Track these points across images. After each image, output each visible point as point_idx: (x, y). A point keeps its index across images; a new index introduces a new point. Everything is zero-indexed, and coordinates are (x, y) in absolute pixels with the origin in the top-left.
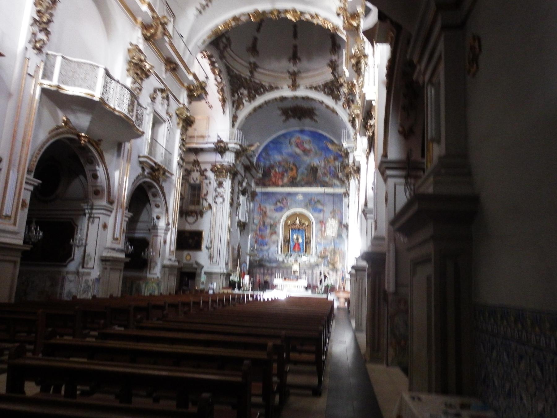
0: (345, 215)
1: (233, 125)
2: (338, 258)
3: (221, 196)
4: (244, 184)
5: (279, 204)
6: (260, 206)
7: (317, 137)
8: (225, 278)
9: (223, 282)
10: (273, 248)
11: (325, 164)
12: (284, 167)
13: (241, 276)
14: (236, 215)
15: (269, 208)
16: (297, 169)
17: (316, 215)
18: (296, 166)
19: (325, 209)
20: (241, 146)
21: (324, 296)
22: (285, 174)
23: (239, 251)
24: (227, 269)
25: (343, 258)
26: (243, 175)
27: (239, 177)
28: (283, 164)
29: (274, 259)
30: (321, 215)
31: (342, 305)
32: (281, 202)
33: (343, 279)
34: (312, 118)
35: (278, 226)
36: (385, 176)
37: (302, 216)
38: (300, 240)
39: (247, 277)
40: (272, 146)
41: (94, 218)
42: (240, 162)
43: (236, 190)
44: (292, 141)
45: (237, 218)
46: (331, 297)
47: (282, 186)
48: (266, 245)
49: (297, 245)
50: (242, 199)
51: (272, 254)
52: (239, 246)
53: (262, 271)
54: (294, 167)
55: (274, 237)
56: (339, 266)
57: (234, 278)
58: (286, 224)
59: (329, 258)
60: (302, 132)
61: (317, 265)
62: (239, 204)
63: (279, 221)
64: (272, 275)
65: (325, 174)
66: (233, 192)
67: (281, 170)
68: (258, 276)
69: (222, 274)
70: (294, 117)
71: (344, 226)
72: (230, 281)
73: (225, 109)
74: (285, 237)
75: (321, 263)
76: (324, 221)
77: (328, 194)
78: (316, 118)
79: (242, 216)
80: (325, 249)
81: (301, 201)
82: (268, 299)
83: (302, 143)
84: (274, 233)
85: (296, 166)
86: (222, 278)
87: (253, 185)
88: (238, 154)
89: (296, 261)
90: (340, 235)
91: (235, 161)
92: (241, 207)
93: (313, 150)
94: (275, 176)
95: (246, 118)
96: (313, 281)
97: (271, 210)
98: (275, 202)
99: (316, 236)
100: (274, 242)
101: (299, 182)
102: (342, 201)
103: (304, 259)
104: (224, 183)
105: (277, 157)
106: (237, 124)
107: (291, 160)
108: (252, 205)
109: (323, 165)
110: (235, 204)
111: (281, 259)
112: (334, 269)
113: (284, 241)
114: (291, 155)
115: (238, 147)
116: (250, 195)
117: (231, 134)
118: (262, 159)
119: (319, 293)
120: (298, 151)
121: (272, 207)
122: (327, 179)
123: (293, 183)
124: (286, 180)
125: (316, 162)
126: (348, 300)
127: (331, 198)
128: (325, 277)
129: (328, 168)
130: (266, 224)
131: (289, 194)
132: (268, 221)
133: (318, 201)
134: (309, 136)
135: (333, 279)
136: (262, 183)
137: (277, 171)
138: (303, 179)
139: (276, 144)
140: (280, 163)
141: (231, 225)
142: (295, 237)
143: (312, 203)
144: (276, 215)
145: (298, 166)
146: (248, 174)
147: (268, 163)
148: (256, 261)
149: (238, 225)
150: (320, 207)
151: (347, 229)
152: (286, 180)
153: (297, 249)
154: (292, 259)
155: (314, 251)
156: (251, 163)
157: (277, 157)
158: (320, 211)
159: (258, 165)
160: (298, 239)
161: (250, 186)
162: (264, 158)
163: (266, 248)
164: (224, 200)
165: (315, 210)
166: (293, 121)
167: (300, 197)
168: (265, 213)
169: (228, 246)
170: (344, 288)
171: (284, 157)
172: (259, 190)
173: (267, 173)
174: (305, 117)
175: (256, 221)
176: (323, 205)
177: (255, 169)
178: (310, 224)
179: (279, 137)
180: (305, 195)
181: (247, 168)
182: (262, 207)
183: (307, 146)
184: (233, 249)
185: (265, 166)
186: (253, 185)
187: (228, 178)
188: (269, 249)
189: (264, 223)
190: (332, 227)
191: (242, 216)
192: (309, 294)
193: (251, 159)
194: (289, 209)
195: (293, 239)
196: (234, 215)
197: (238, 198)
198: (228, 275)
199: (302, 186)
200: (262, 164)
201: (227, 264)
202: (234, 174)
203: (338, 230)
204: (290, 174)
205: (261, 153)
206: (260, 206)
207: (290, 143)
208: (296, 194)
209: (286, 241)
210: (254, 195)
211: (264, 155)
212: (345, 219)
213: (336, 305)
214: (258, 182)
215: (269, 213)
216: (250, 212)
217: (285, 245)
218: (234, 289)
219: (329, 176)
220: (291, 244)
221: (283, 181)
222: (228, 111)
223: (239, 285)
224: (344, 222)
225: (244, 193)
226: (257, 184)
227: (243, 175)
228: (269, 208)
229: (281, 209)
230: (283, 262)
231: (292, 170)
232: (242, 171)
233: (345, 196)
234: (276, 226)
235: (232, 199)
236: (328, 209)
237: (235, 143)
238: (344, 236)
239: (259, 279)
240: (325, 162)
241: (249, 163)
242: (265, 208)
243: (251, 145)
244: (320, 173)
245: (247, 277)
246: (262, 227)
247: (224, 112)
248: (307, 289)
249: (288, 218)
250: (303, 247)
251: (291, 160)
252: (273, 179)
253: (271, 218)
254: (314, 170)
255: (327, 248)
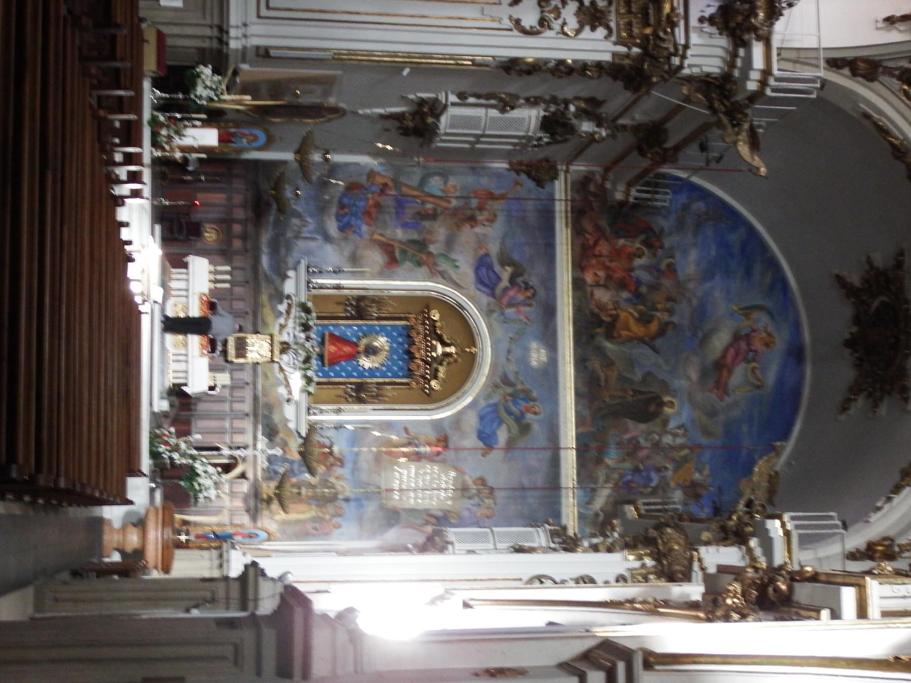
0: (477, 538)
1: (835, 63)
2: (301, 513)
3: (543, 22)
4: (587, 127)
5: (506, 274)
6: (492, 197)
7: (777, 414)
8: (206, 44)
9: (190, 36)
10: (331, 255)
11: (673, 448)
12: (653, 287)
13: (214, 117)
14: (462, 96)
15: (491, 235)
16: (648, 342)
17: (472, 421)
18: (662, 332)
19: (496, 455)
20: (754, 97)
21: (146, 463)
22: (625, 295)
23: (317, 111)
24: (244, 54)
25: (303, 535)
26: (621, 121)
27: (617, 98)
28: (667, 283)
29: (291, 261)
30: (471, 441)
31: (110, 539)
32: (515, 283)
33: (219, 541)
34: (855, 390)
35: (424, 270)
36: (583, 666)
37: (466, 365)
38: (366, 363)
39: (209, 137)
40: (735, 238)
41: (219, 548)
42: (687, 99)
43: (569, 89)
44: (756, 315)
45: (453, 98)
46: (139, 489)
47: (578, 284)
48: (342, 229)
49: (347, 349)
50: (529, 117)
51: (308, 253)
52: (335, 111)
53: (239, 214)
54: (654, 327)
55: (376, 257)
56: (273, 520)
57: (207, 84)
58: (426, 303)
59: (305, 480)
60: (796, 354)
61: (271, 433)
62: (506, 105)
63: (436, 273)
64: (221, 254)
65: (632, 449)
66: (562, 70)
67: (644, 276)
68: (218, 198)
69: (222, 30)
70: (857, 320)
71: (438, 533)
72: (194, 68)
73: (902, 26)
74: (378, 301)
75: (284, 446)
76: (450, 455)
77: (555, 463)
78: (861, 402)
79: (456, 122)
80: (341, 462)
81: (524, 361)
82: (129, 243)
83: (751, 356)
84: (393, 259)
85: (662, 332)
86: (208, 32)
87: (579, 168)
88: (720, 89)
89: (285, 348)
90: (392, 516)
91: (690, 79)
92: (494, 113)
93: (729, 400)
94: (617, 253)
95: (867, 116)
96: (208, 416)
97: (481, 242)
98: (516, 257)
99: (387, 426)
100: (354, 259)
101: (600, 351)
102: (533, 522)
103: (296, 380)
104: (601, 32)
105: (690, 263)
106: (834, 77)
107: (682, 315)
108: (501, 165)
109: (668, 440)
110: (514, 86)
111: (289, 287)
112: (257, 503)
113: (360, 299)
114: (701, 314)
115: (752, 86)
116: (540, 155)
117: (800, 56)
118: (683, 198)
119: (155, 438)
120: (720, 341)
121: (494, 248)
122: (612, 458)
123: (589, 326)
124: (603, 296)
125: (678, 413)
126: (132, 564)
127: (540, 480)
128: (227, 468)
129: (658, 460)
130: (427, 224)
131: (549, 312)
132: (440, 231)
133: (525, 429)
134: (781, 380)
135: (220, 500)
136: (588, 203)
137: (638, 262)
138: (609, 364)
139: (745, 254)
140: (672, 270)
141: (425, 69)
142: (381, 341)
143: (517, 406)
144: (465, 268)
145: (658, 343)
146: (625, 140)
147: (663, 223)
148: (278, 186)
149: (422, 102)
150: (502, 436)
151: (423, 549)
152: (603, 296)
153: (331, 348)
154: (291, 332)
155: (327, 417)
156: (670, 156)
157: (690, 263)
158: (487, 439)
159: (655, 183)
160: (371, 351)
161: (577, 154)
162: (685, 207)
163: (332, 227)
164: (526, 32)
165: (488, 419)
166: (841, 318)
167: (537, 356)
168: (472, 220)
169: (339, 59)
170: (180, 545)
171: (691, 286)
172: (560, 188)
173: (628, 219)
174: (858, 365)
175: (435, 185)
176: (510, 446)
177: (646, 172)
178: (429, 398)
179: (773, 264)
180: (550, 372)
181: (651, 139)
182: (497, 205)
183: (738, 376)
184: (327, 83)
185: (657, 211)
186: (579, 168)
187: (622, 49)
188: (327, 238)
189: (433, 216)
190: (421, 484)
191: (460, 119)
192: (152, 400)
193: (692, 151)
194: (488, 313)
195: (371, 332)
196: (464, 85)
197: (532, 102)
198: (219, 60)
199: (580, 362)
200: (664, 199)
201: (264, 54)
202: (630, 75)
203: (412, 511)
204: (628, 315)
205: (705, 194)
206: (492, 197)
207: (747, 311)
208: (550, 341)
209: (360, 307)
210: (540, 172)
211: (699, 206)
212: (463, 539)
213: (113, 513)
214: (592, 188)
215: (467, 234)
216: (473, 155)
217: (345, 302)
218: (157, 83)
219: (628, 465)
220: (349, 328)
221: (597, 285)
222: (895, 36)
223: (179, 104)
224: (451, 533)
225: (555, 125)
226: (582, 185)
227: (621, 121)
228: (491, 235)
229: (485, 277)
230: (279, 296)
231: (645, 320)
232: (639, 116)
233: (553, 534)
234: (419, 264)
235: (534, 69)
236: (497, 468)
237: (767, 72)
238: (392, 535)
239: (210, 201)
240: (682, 447)
241: (670, 144)
242: (492, 220)
243: (754, 144)
244: (636, 429)
245: (209, 137)
246: (410, 212)
247: (890, 21)
248: (177, 393)
249: (454, 312)
250: (342, 375)
251: (682, 315)
252: (603, 248)
253: (450, 243)
254: (647, 407)
255: (339, 471)
